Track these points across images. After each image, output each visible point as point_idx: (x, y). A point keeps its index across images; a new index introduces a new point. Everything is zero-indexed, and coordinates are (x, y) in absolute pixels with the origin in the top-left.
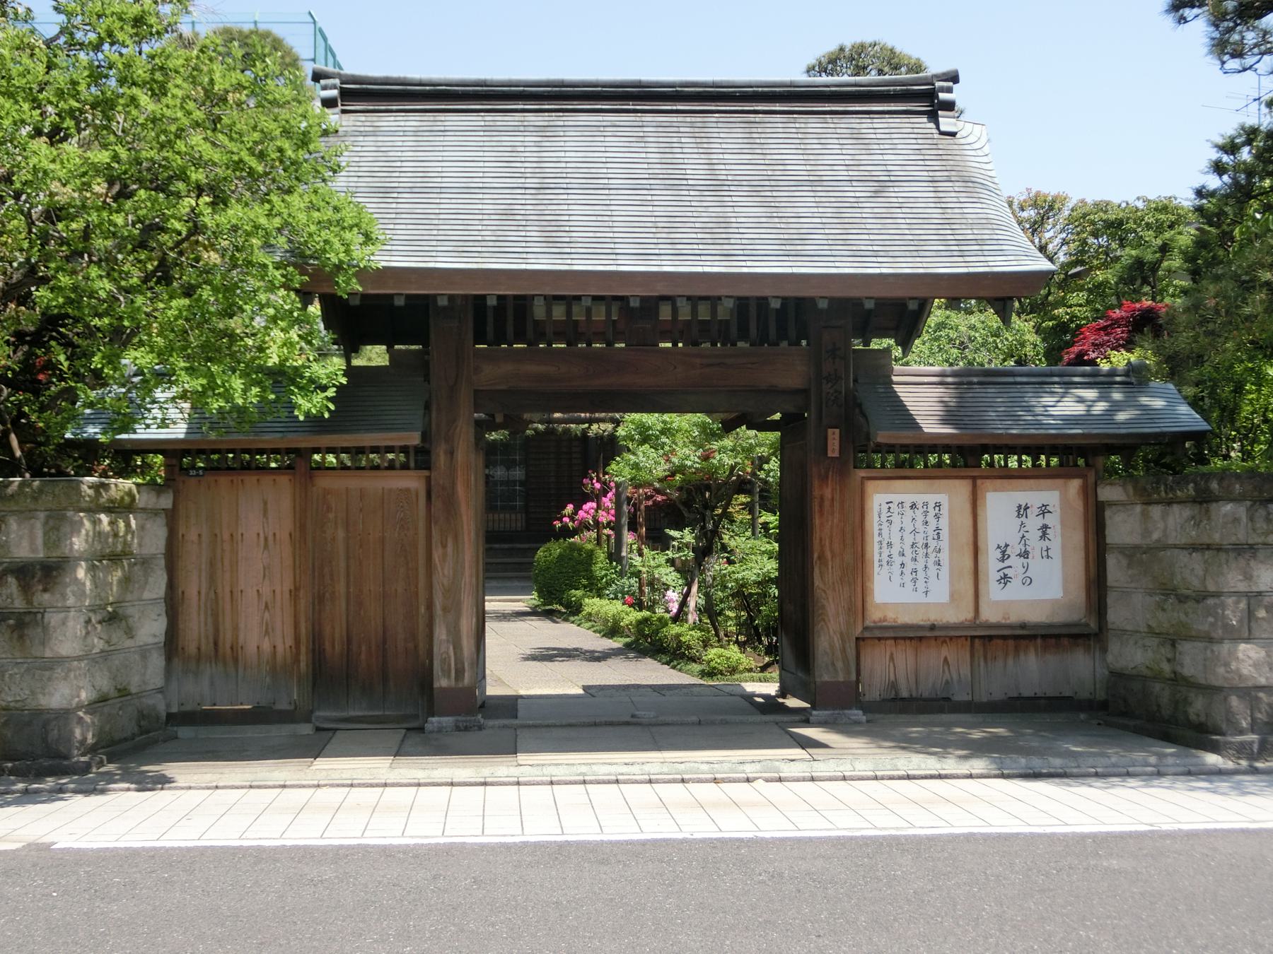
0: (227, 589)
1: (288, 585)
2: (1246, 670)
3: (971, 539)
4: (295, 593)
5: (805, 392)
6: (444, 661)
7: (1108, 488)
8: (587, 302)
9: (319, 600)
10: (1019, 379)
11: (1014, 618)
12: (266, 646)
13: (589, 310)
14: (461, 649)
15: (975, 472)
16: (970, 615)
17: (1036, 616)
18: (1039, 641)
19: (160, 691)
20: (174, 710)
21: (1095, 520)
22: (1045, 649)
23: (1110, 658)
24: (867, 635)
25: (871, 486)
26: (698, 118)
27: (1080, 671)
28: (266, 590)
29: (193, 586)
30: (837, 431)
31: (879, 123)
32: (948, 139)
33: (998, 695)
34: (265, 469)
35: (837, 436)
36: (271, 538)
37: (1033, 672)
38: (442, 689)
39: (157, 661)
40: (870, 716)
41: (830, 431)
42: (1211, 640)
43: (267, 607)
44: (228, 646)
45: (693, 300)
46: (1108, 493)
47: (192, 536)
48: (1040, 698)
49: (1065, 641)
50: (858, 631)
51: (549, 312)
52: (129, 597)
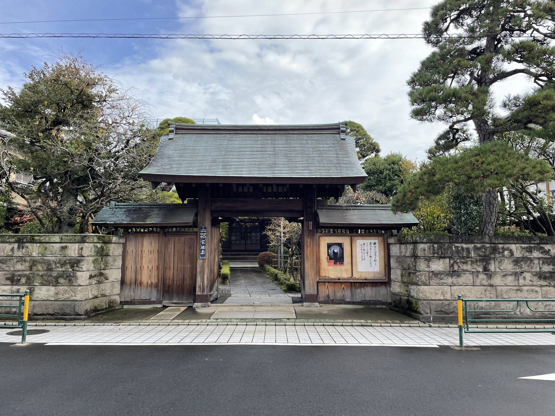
1: (156, 264)
2: (428, 295)
4: (158, 268)
6: (199, 287)
8: (248, 186)
9: (165, 269)
11: (363, 277)
12: (150, 282)
13: (248, 188)
16: (350, 276)
17: (370, 277)
19: (118, 295)
20: (123, 300)
21: (387, 248)
23: (392, 289)
25: (321, 238)
26: (273, 136)
27: (381, 294)
28: (150, 267)
29: (130, 264)
31: (323, 136)
32: (343, 141)
33: (359, 300)
37: (368, 293)
38: (198, 295)
39: (118, 286)
40: (321, 305)
42: (418, 285)
45: (278, 185)
46: (391, 240)
47: (130, 251)
49: (358, 285)
51: (238, 189)
52: (493, 256)
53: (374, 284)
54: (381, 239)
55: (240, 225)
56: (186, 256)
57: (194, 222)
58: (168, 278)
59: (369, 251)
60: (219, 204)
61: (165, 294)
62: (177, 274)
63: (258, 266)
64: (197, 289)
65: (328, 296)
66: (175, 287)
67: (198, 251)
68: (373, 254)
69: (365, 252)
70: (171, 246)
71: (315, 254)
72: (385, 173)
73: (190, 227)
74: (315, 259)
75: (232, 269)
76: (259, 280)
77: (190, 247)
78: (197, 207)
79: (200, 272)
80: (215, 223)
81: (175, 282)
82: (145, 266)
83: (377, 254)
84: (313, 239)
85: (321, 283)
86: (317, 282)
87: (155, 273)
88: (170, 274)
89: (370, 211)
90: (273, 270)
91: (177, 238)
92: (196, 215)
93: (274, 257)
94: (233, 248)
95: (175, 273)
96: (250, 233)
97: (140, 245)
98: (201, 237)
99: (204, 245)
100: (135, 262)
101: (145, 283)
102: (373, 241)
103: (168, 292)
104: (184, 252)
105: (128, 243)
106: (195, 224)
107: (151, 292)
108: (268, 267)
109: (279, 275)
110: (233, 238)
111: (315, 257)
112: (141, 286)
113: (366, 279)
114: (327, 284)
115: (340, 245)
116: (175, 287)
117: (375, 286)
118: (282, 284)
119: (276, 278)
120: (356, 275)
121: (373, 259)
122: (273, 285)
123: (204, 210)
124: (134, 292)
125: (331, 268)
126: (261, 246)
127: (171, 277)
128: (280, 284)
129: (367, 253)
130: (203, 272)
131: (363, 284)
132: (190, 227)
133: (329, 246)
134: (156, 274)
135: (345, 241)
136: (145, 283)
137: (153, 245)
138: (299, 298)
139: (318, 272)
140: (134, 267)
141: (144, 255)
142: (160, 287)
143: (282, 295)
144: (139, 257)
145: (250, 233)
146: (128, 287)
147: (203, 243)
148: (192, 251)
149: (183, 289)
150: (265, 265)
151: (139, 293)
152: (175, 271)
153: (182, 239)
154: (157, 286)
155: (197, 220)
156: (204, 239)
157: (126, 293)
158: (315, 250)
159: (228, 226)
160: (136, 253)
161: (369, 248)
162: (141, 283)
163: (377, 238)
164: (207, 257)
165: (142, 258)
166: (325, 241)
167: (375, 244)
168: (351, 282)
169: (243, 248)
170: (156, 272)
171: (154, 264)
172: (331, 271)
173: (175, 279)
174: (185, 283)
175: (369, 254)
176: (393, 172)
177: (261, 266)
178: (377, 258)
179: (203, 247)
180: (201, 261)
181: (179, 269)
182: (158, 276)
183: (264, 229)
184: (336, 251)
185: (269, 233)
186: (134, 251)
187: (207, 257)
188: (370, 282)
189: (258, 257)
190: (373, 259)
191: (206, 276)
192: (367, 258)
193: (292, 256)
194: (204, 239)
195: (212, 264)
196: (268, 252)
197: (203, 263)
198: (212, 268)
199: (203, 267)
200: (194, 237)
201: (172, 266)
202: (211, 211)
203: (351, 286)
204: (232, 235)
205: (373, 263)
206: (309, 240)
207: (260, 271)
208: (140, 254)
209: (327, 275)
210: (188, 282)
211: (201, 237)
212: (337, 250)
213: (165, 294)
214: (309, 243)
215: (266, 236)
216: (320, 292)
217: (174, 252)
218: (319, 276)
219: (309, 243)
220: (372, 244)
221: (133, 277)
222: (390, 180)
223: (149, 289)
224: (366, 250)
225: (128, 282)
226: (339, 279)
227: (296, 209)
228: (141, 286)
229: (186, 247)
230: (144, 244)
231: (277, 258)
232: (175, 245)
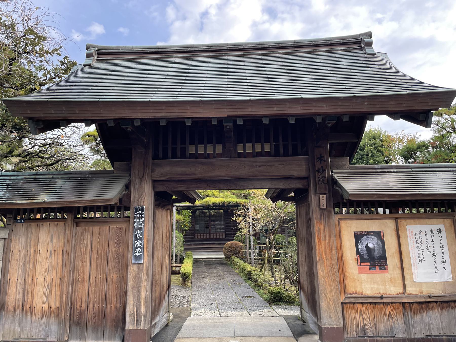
0: (30, 279)
1: (59, 275)
3: (398, 250)
5: (307, 178)
7: (295, 175)
10: (380, 170)
11: (426, 291)
12: (47, 307)
14: (140, 309)
15: (396, 216)
17: (437, 291)
18: (438, 303)
22: (442, 308)
24: (347, 301)
25: (343, 223)
28: (49, 280)
30: (325, 196)
32: (371, 58)
34: (36, 220)
35: (325, 198)
36: (53, 252)
38: (130, 331)
41: (321, 196)
43: (48, 286)
44: (28, 306)
47: (16, 252)
48: (442, 336)
50: (342, 299)
53: (446, 305)
54: (448, 222)
55: (203, 212)
56: (111, 258)
57: (121, 200)
58: (79, 299)
59: (430, 244)
60: (167, 169)
61: (74, 328)
62: (96, 290)
63: (223, 256)
64: (128, 319)
65: (363, 329)
66: (90, 314)
67: (130, 249)
68: (438, 250)
69: (424, 246)
70: (87, 242)
71: (334, 252)
72: (366, 148)
73: (111, 208)
74: (335, 261)
75: (196, 262)
76: (228, 279)
77: (118, 243)
78: (130, 175)
79: (133, 288)
80: (163, 200)
81: (91, 306)
82: (40, 277)
83: (446, 249)
84: (329, 226)
85: (349, 306)
86: (342, 303)
87: (56, 290)
88: (82, 291)
89: (413, 174)
90: (243, 264)
91: (96, 229)
92: (128, 187)
93: (241, 247)
94: (197, 237)
95: (92, 289)
96: (214, 221)
97: (33, 242)
98: (136, 225)
99: (141, 239)
100: (24, 271)
101: (39, 308)
102: (436, 227)
103: (78, 323)
104: (108, 252)
105: (13, 238)
106: (123, 205)
107: (48, 326)
108: (236, 259)
109: (254, 273)
110: (197, 227)
111: (335, 257)
112: (31, 313)
113: (430, 297)
114: (359, 306)
115: (378, 235)
116: (90, 314)
117: (448, 307)
118: (260, 287)
119: (249, 276)
120: (411, 290)
121: (439, 258)
122: (246, 288)
123: (142, 179)
124: (20, 324)
125: (364, 276)
126: (225, 235)
127: (85, 297)
128: (256, 286)
129: (428, 248)
130: (137, 288)
131: (424, 306)
132: (111, 208)
133: (358, 237)
134: (58, 293)
135: (387, 227)
136: (39, 308)
137: (55, 241)
138: (297, 318)
139: (343, 285)
140: (21, 279)
141: (39, 258)
142: (65, 314)
143: (266, 311)
144: (30, 261)
145: (214, 221)
146: (11, 316)
147: (139, 236)
148: (121, 249)
149: (104, 319)
150: (232, 257)
151: (29, 326)
152: (92, 285)
153: (106, 228)
154: (58, 314)
155: (129, 196)
156: (140, 229)
157: (6, 326)
158: (334, 245)
159: (191, 214)
160: (25, 255)
161: (430, 239)
162: (32, 310)
163: (441, 220)
164: (145, 260)
165: (35, 265)
166: (350, 227)
167: (439, 231)
168: (404, 303)
169: (208, 237)
170: (58, 289)
171: (56, 274)
172: (367, 283)
173: (91, 301)
174: (109, 307)
175: (431, 249)
176: (376, 148)
177: (228, 257)
178: (447, 257)
179: (138, 243)
180: (135, 267)
181: (98, 281)
182: (61, 296)
183: (232, 215)
184: (370, 245)
185: (239, 219)
186: (23, 252)
187: (145, 260)
188: (436, 302)
189: (225, 246)
190: (439, 258)
191: (143, 295)
192: (429, 258)
193: (270, 248)
194: (140, 229)
195: (158, 269)
196: (234, 242)
197: (139, 271)
198: (157, 277)
199: (138, 278)
200: (124, 226)
201: (87, 277)
202: (154, 181)
203: (404, 309)
204: (196, 224)
205: (440, 266)
206: (322, 227)
207: (226, 263)
208: (32, 257)
209: (359, 290)
210: (113, 305)
211: (136, 225)
212: (373, 243)
213: (74, 328)
214: (322, 232)
215: (236, 223)
216: (348, 322)
217: (91, 251)
218: (345, 292)
219: (322, 232)
220: (435, 232)
221: (19, 297)
222: (372, 156)
223: (45, 320)
224: (424, 242)
225: (11, 307)
226: (382, 297)
227: (296, 174)
228: (31, 313)
229: (111, 244)
230: (40, 240)
231: (245, 249)
232: (94, 240)
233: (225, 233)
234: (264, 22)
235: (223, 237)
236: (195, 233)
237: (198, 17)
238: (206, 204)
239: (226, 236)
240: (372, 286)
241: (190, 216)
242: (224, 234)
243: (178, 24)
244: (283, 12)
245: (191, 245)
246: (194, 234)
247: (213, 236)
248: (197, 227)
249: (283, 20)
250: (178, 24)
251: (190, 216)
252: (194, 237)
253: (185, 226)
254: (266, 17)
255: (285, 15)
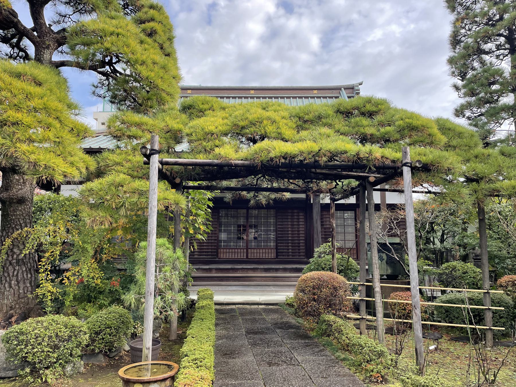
94: (223, 256)
110: (223, 236)
126: (277, 253)
159: (211, 204)
169: (243, 256)
204: (220, 231)
233: (277, 249)
234: (279, 17)
235: (273, 255)
236: (218, 247)
237: (205, 9)
238: (264, 157)
239: (277, 256)
240: (474, 327)
241: (209, 207)
242: (274, 251)
243: (182, 16)
244: (300, 7)
245: (210, 270)
246: (217, 249)
247: (254, 254)
248: (223, 236)
249: (301, 15)
250: (182, 16)
251: (209, 207)
252: (217, 255)
253: (197, 230)
254: (282, 11)
255: (303, 10)
